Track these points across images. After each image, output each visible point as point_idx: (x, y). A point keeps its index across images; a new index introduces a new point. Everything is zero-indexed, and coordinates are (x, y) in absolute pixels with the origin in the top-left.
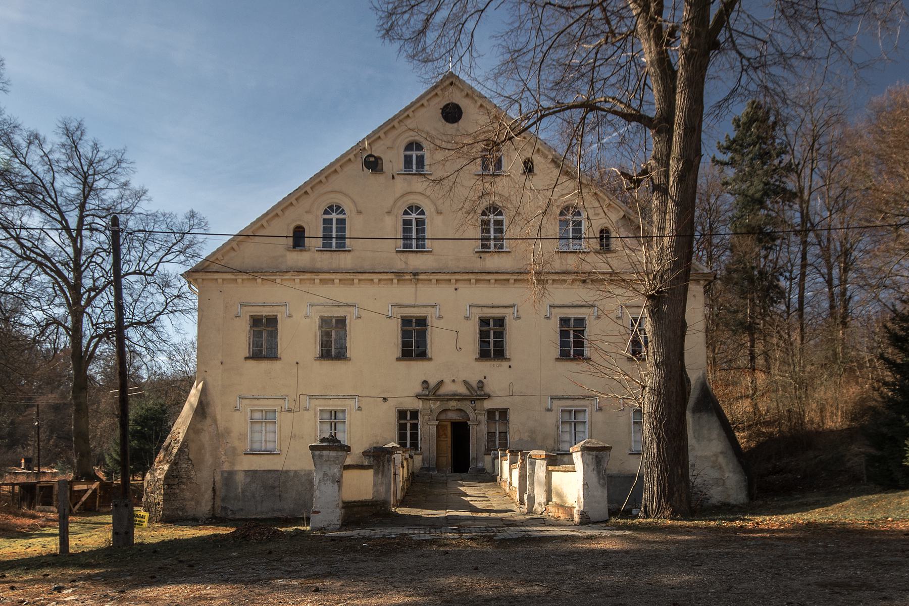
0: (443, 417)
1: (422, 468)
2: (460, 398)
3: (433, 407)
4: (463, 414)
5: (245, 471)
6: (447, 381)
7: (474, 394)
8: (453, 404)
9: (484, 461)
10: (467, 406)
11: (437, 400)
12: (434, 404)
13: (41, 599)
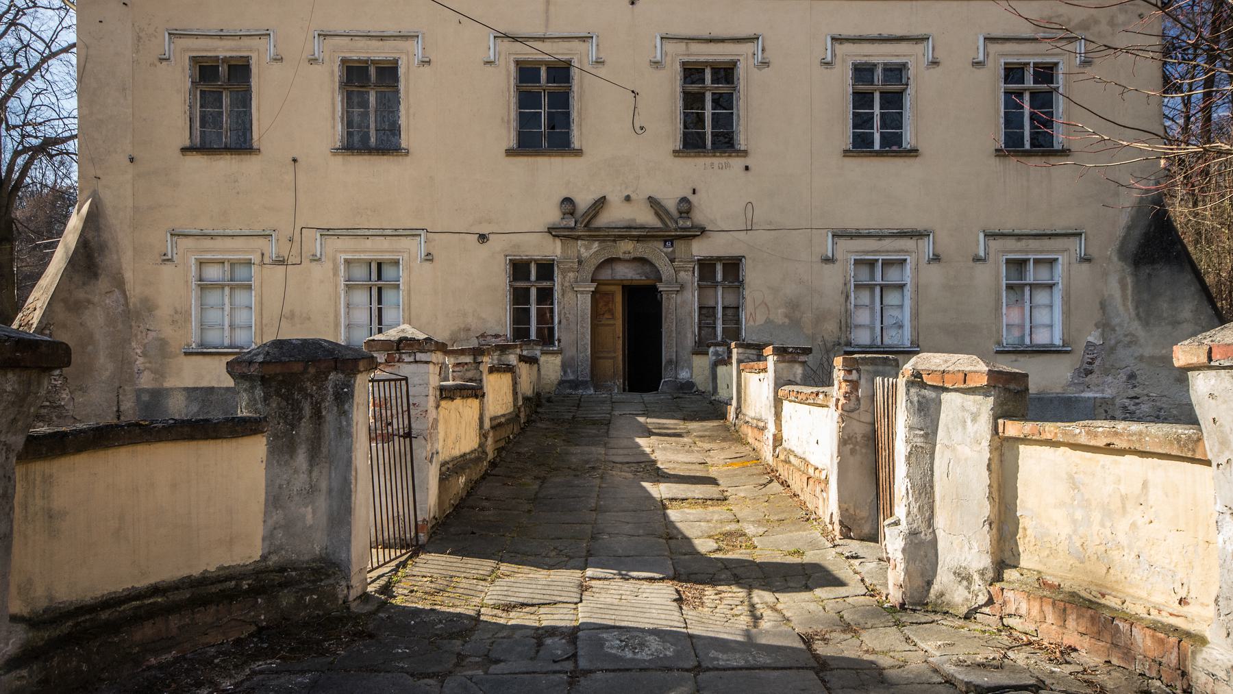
0: (606, 274)
3: (585, 254)
4: (647, 268)
6: (614, 198)
9: (691, 368)
10: (656, 252)
11: (593, 238)
12: (587, 248)
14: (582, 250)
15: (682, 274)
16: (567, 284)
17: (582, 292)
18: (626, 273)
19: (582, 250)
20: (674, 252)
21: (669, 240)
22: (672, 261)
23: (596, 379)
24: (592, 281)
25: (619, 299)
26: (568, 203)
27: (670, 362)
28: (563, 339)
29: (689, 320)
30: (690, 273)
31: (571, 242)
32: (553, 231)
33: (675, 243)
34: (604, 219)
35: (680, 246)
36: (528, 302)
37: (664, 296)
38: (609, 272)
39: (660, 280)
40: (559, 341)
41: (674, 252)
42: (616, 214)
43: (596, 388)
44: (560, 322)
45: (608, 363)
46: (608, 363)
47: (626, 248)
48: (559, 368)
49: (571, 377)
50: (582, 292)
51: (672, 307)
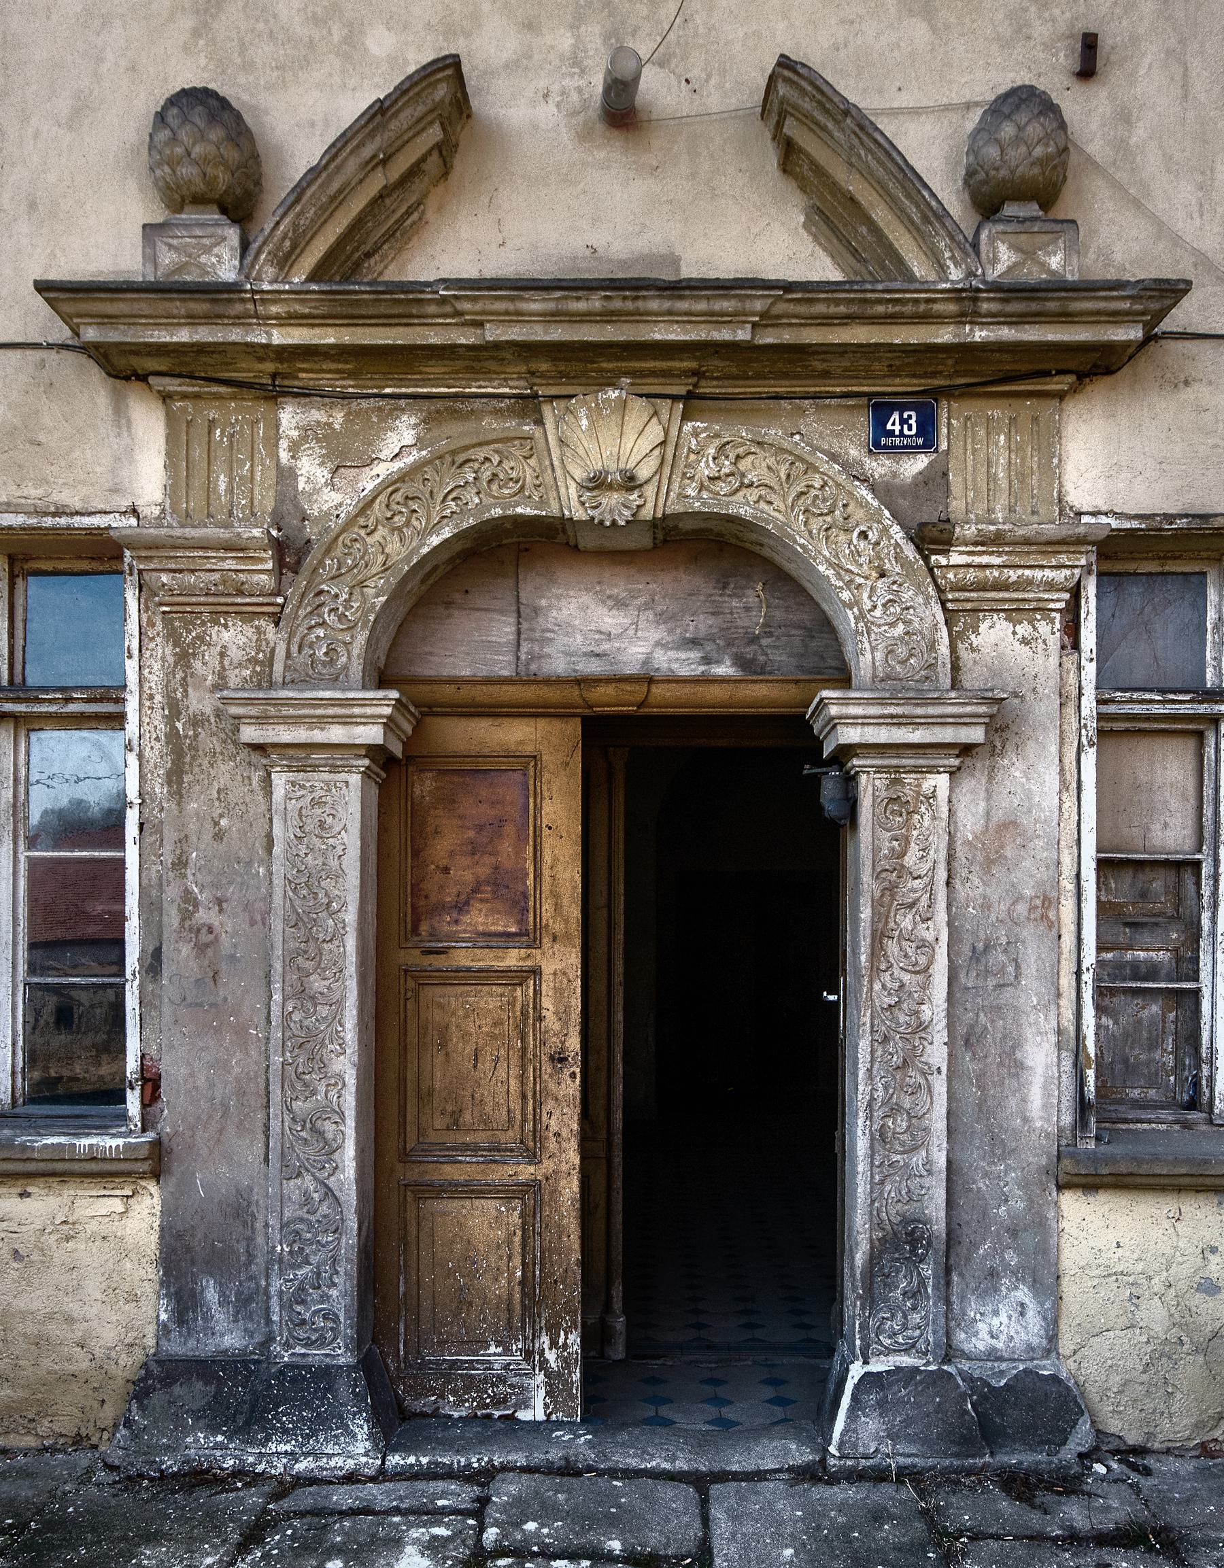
0: (476, 646)
1: (158, 1377)
2: (731, 359)
3: (326, 493)
4: (750, 606)
5: (637, 78)
6: (532, 97)
7: (926, 267)
8: (606, 450)
9: (1045, 1279)
10: (813, 483)
11: (378, 373)
12: (344, 457)
13: (670, 1523)
14: (310, 470)
15: (995, 636)
16: (200, 702)
17: (301, 757)
18: (610, 632)
19: (310, 470)
20: (936, 480)
21: (916, 387)
22: (931, 538)
23: (397, 1368)
24: (383, 682)
25: (559, 810)
26: (207, 154)
27: (903, 1240)
28: (172, 1070)
29: (1032, 955)
30: (1049, 632)
31: (233, 415)
32: (117, 336)
33: (949, 419)
34: (458, 247)
35: (979, 453)
36: (121, 845)
37: (871, 786)
38: (503, 630)
39: (843, 678)
40: (151, 1097)
41: (936, 480)
42: (534, 216)
43: (395, 1422)
44: (153, 964)
45: (487, 1225)
46: (487, 1225)
47: (607, 449)
48: (144, 1274)
49: (230, 1338)
50: (301, 757)
51: (925, 859)
